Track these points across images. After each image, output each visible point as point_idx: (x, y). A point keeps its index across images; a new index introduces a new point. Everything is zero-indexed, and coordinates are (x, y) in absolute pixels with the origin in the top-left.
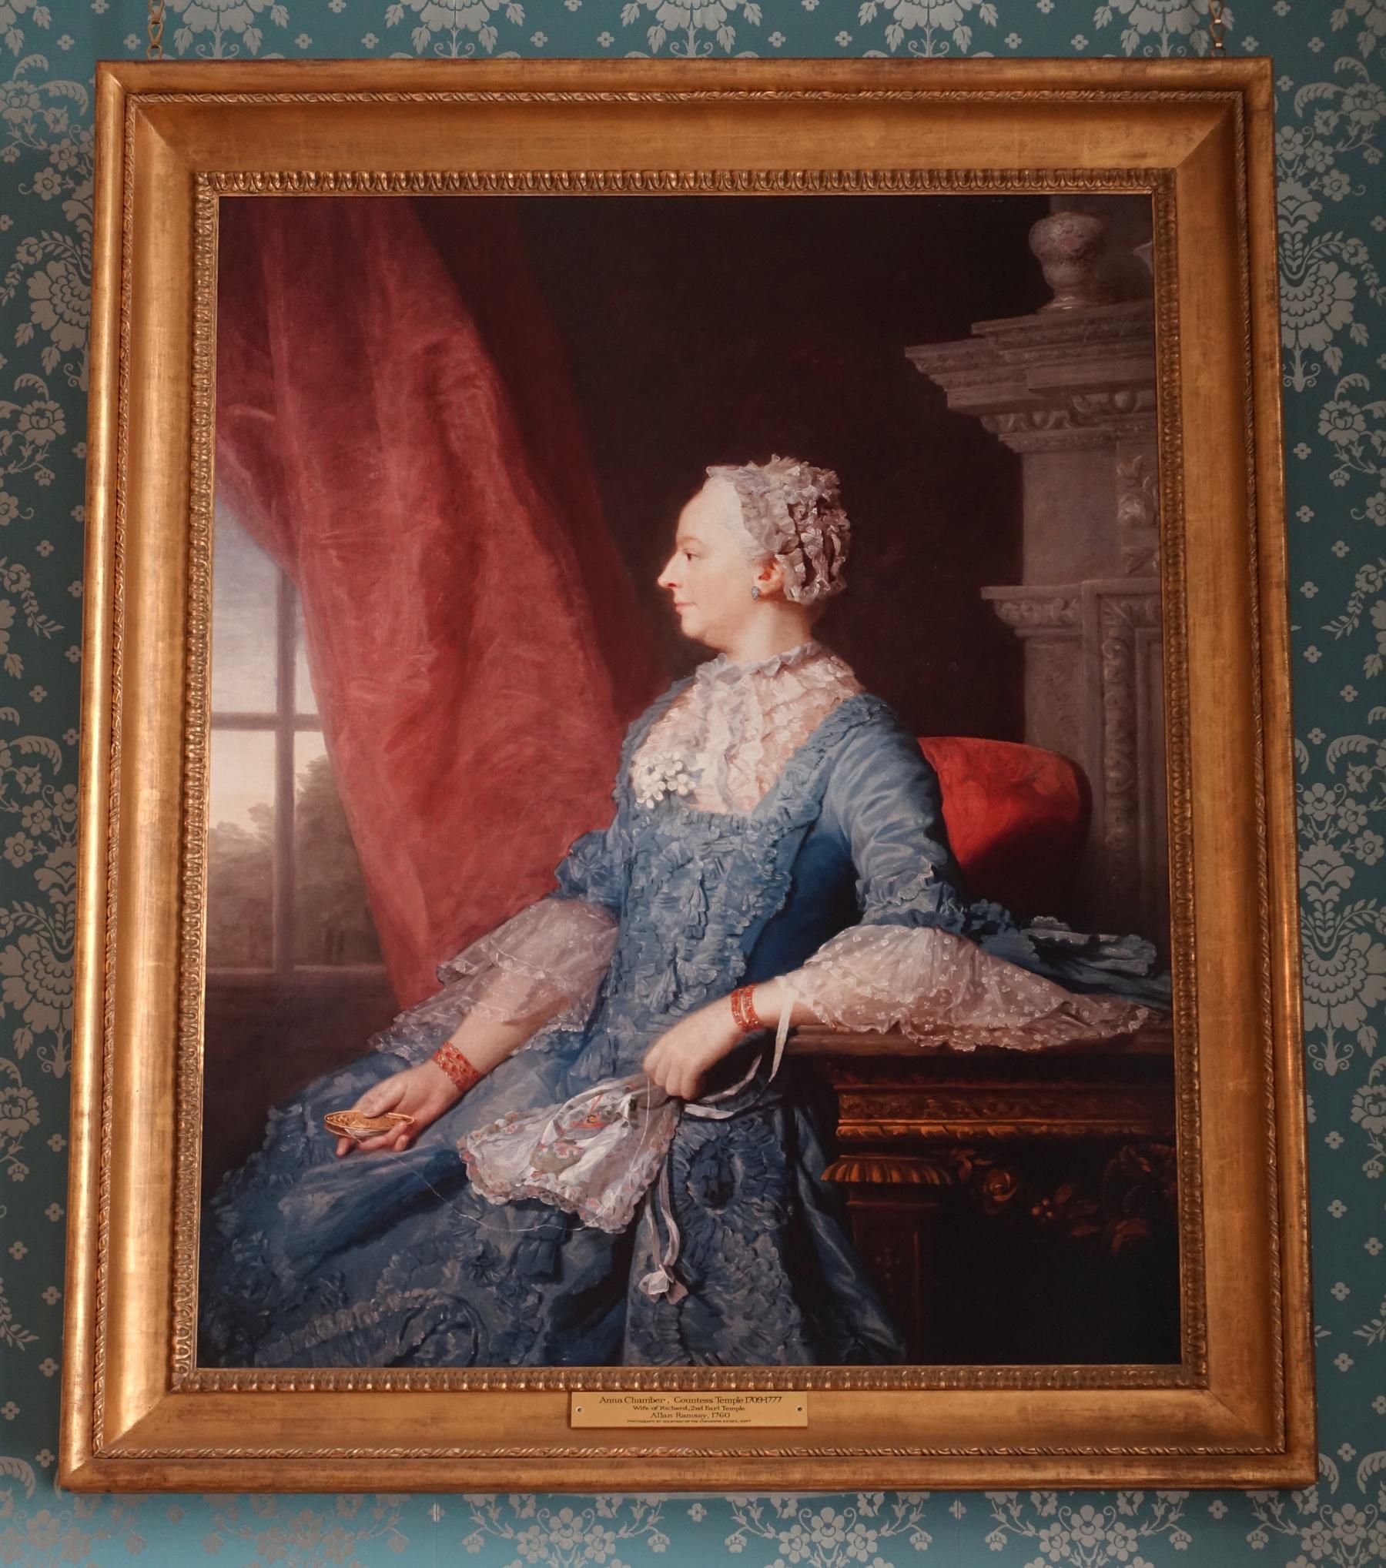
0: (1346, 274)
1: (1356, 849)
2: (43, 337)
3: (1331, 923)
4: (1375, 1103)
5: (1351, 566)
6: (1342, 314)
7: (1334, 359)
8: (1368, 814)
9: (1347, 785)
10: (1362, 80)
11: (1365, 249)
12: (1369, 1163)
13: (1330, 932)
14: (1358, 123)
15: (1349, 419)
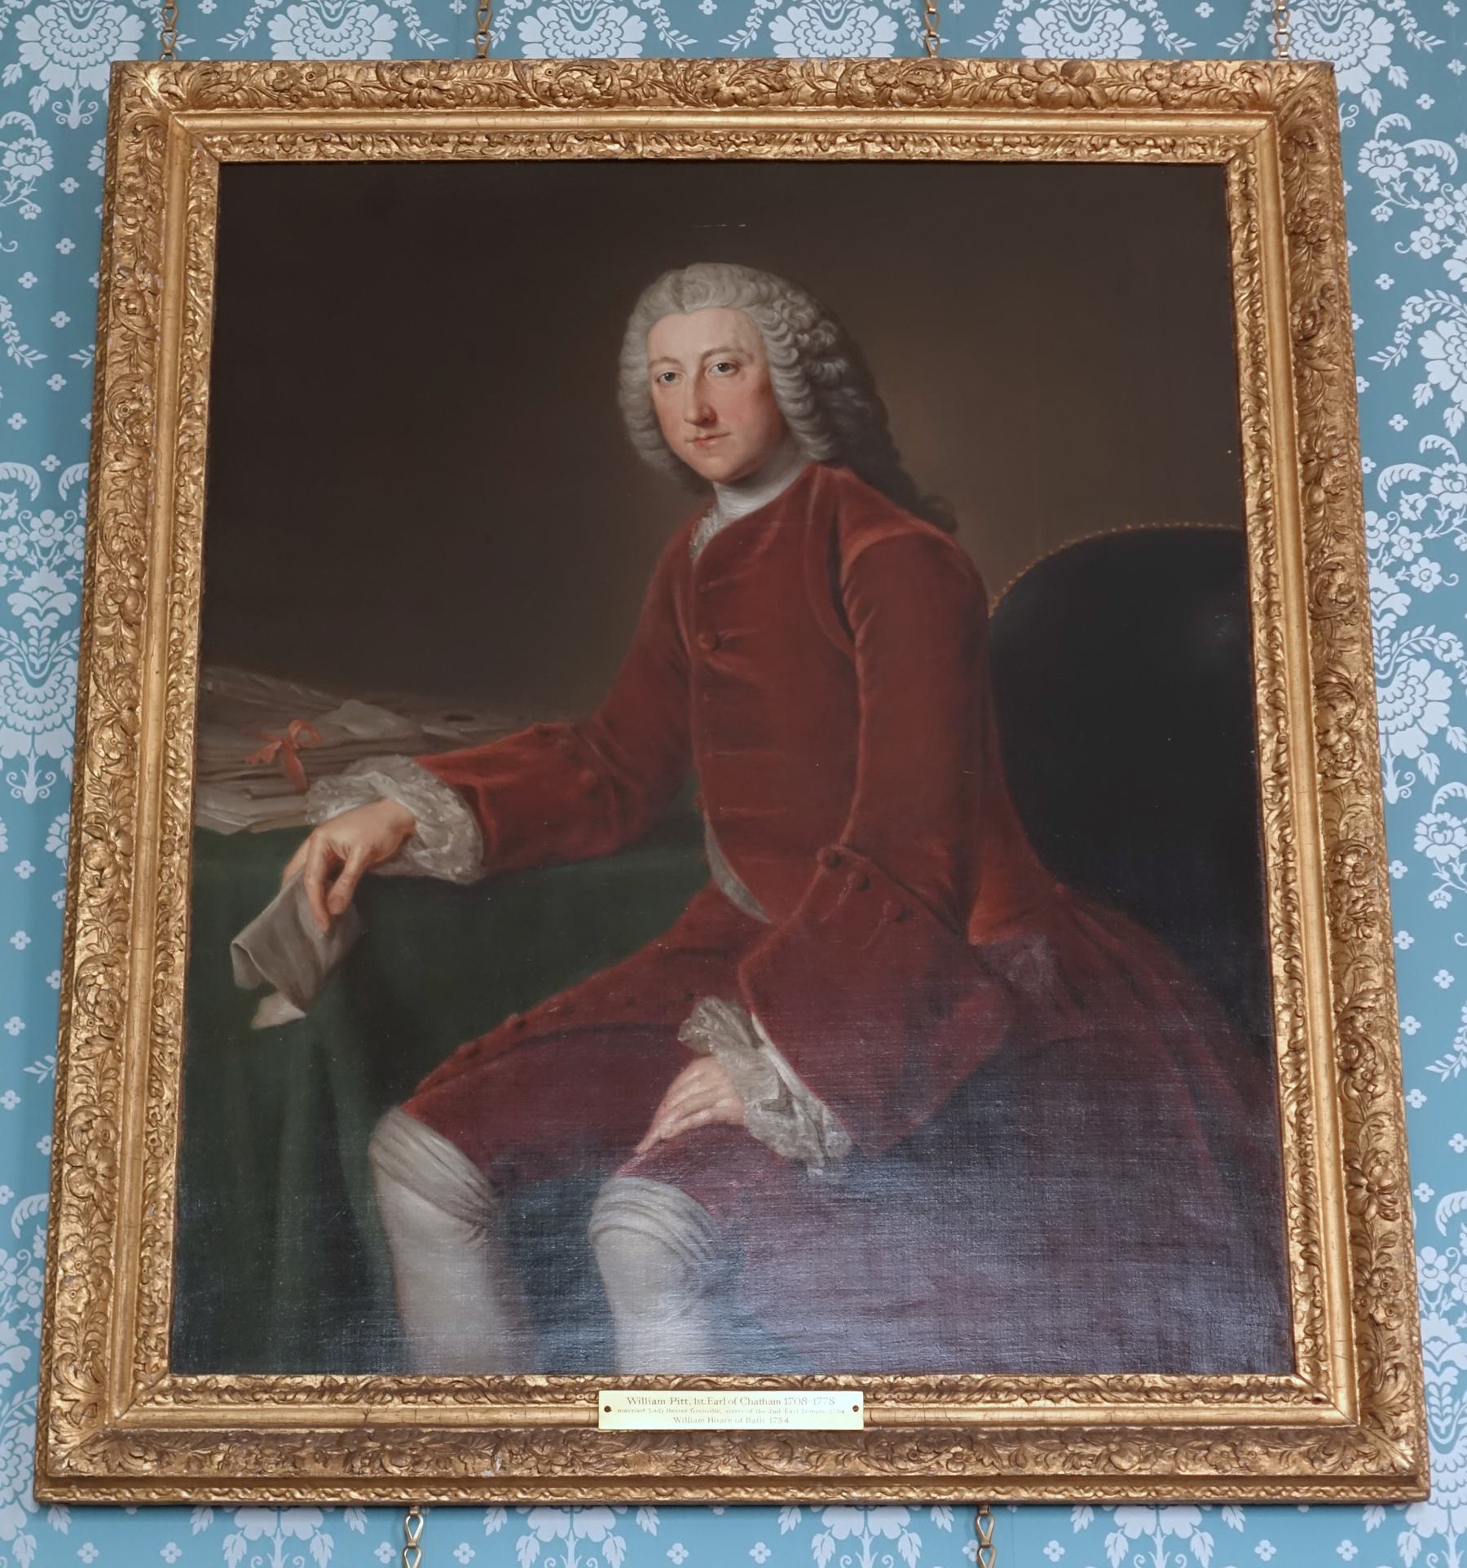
0: (1439, 673)
1: (1411, 576)
2: (32, 78)
3: (1387, 650)
4: (1440, 831)
5: (1396, 298)
6: (1379, 58)
7: (1430, 766)
8: (1424, 542)
9: (1400, 513)
10: (1450, 459)
11: (1460, 644)
12: (1436, 893)
13: (1448, 1421)
14: (1448, 506)
15: (1391, 157)
